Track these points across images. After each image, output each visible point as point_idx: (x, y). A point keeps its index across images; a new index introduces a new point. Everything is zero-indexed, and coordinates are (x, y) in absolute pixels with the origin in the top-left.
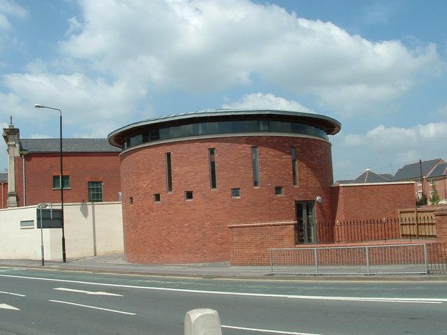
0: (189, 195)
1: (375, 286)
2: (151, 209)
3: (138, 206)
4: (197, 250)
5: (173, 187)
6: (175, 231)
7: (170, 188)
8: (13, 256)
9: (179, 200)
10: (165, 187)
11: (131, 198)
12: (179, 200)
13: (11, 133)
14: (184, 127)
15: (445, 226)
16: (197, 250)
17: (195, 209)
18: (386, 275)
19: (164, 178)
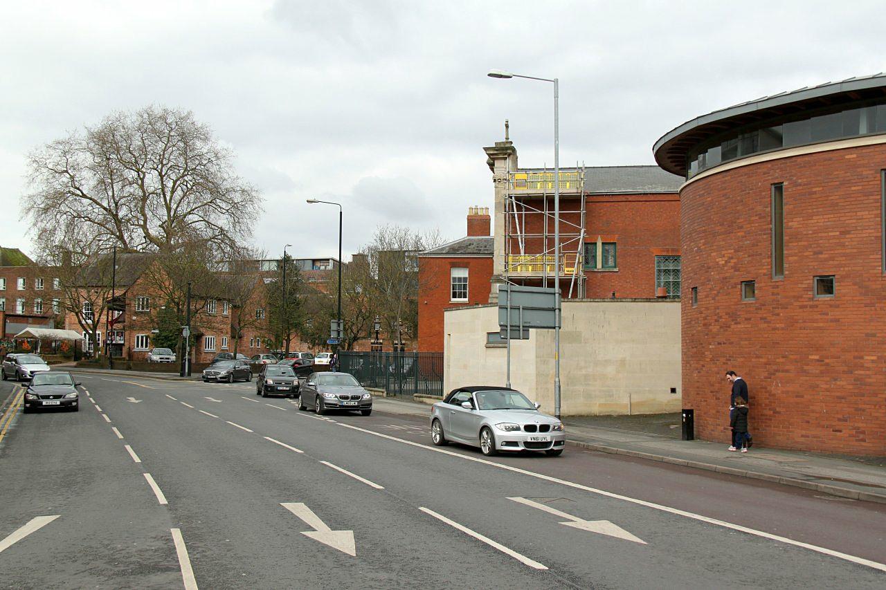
0: (826, 284)
1: (598, 441)
2: (734, 317)
3: (707, 309)
4: (839, 420)
5: (785, 265)
6: (787, 371)
7: (780, 269)
8: (35, 415)
9: (798, 298)
10: (765, 266)
11: (695, 289)
12: (798, 298)
13: (501, 153)
14: (858, 149)
15: (2, 289)
16: (839, 420)
17: (838, 321)
18: (420, 397)
19: (766, 246)
